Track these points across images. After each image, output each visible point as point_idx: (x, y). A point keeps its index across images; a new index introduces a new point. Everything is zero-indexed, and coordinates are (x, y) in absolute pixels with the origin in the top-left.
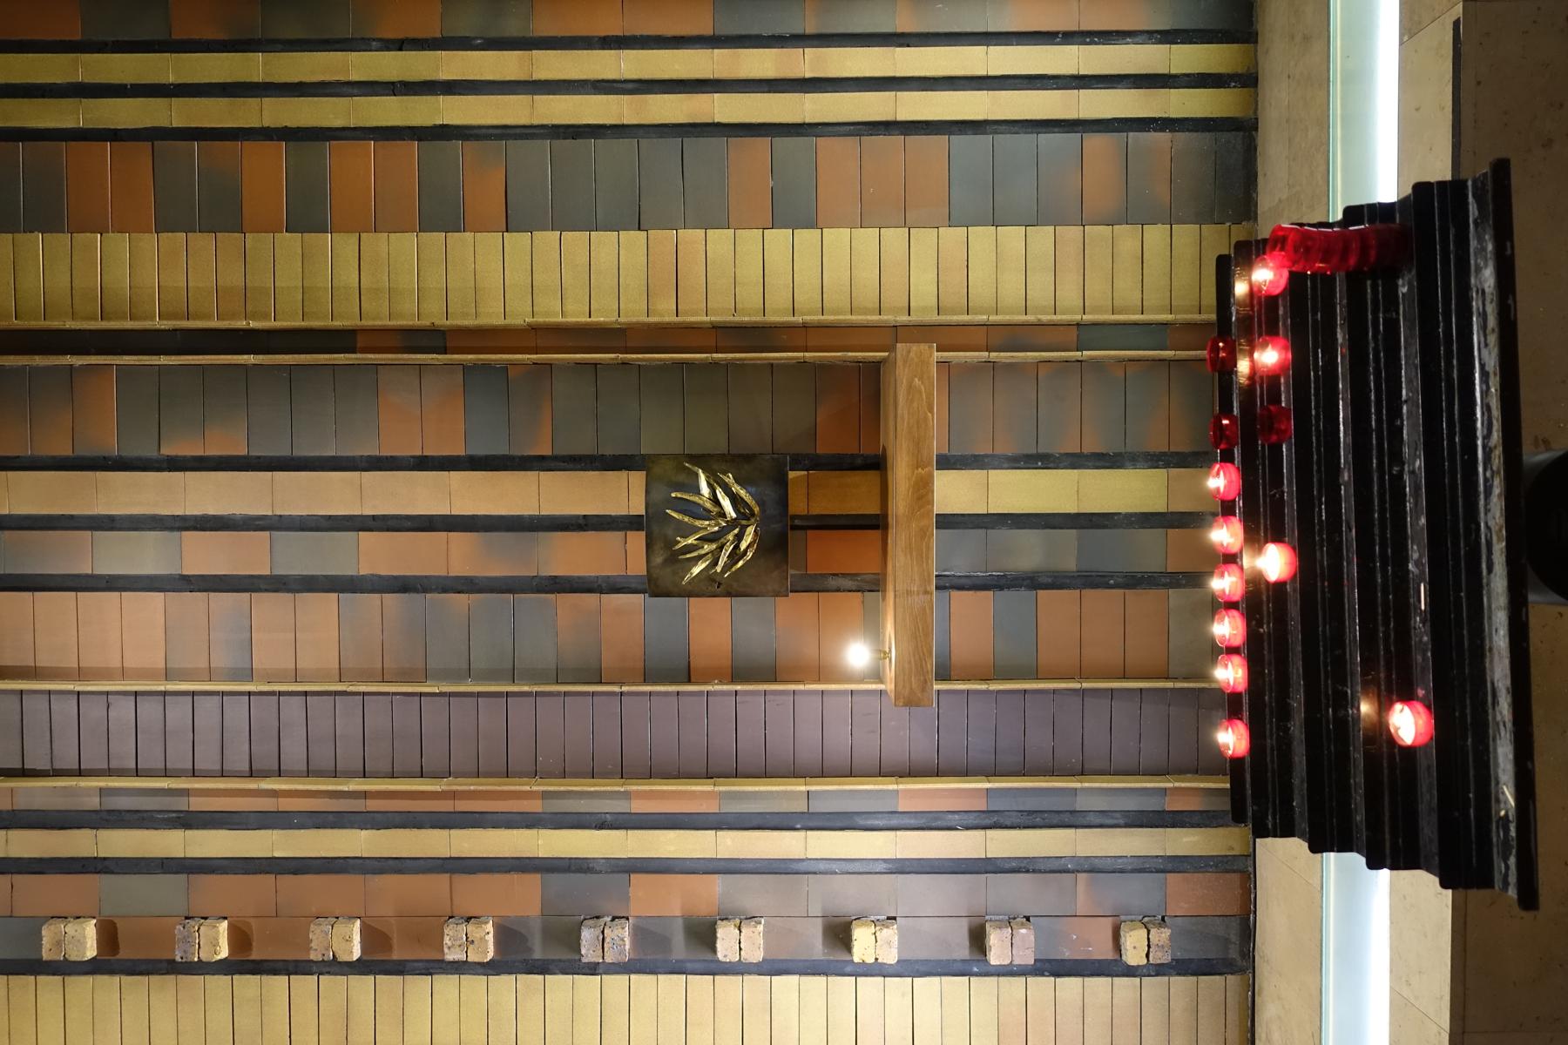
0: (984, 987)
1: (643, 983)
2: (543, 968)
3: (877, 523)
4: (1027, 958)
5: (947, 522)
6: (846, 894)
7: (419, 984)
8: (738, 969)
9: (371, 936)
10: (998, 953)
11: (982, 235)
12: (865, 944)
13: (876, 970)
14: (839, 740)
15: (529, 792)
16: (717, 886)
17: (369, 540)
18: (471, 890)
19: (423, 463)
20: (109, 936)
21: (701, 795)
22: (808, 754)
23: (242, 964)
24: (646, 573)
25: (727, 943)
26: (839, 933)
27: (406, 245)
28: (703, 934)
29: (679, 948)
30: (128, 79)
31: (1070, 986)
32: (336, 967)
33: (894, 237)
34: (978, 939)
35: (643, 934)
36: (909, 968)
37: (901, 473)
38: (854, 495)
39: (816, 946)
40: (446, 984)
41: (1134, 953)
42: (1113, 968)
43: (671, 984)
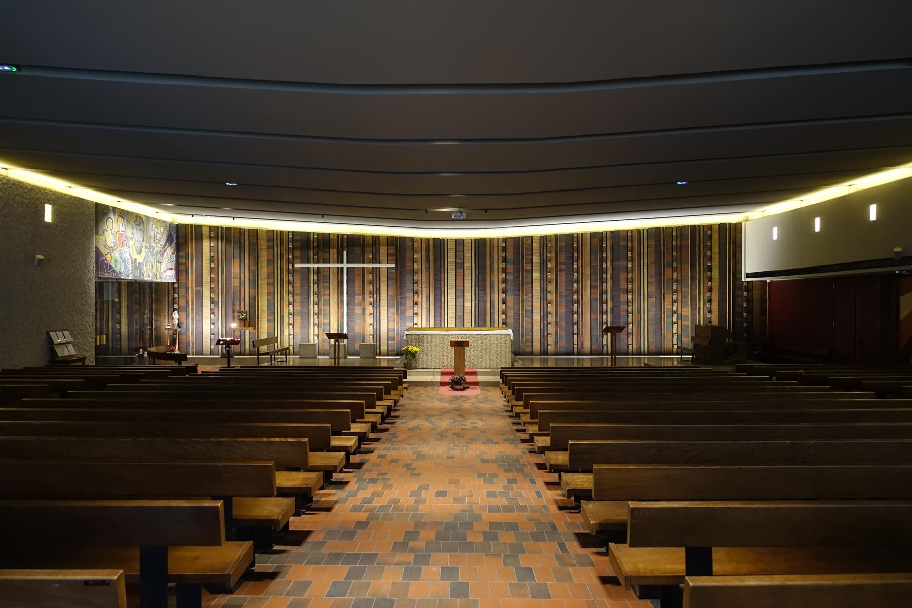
0: (209, 334)
1: (209, 309)
2: (211, 301)
3: (245, 327)
4: (212, 338)
5: (245, 331)
6: (216, 324)
7: (209, 291)
8: (211, 316)
9: (213, 288)
10: (212, 336)
11: (266, 335)
12: (213, 326)
13: (211, 316)
14: (228, 324)
15: (224, 300)
16: (217, 314)
17: (243, 288)
18: (217, 296)
19: (249, 292)
20: (213, 267)
21: (224, 313)
22: (227, 321)
23: (210, 246)
24: (331, 250)
25: (213, 315)
26: (213, 324)
27: (266, 291)
28: (213, 313)
29: (212, 312)
30: (248, 295)
31: (209, 341)
32: (210, 285)
33: (266, 328)
34: (213, 334)
35: (213, 309)
36: (211, 329)
37: (248, 328)
38: (247, 324)
39: (212, 322)
40: (209, 293)
41: (212, 346)
42: (211, 345)
43: (209, 311)
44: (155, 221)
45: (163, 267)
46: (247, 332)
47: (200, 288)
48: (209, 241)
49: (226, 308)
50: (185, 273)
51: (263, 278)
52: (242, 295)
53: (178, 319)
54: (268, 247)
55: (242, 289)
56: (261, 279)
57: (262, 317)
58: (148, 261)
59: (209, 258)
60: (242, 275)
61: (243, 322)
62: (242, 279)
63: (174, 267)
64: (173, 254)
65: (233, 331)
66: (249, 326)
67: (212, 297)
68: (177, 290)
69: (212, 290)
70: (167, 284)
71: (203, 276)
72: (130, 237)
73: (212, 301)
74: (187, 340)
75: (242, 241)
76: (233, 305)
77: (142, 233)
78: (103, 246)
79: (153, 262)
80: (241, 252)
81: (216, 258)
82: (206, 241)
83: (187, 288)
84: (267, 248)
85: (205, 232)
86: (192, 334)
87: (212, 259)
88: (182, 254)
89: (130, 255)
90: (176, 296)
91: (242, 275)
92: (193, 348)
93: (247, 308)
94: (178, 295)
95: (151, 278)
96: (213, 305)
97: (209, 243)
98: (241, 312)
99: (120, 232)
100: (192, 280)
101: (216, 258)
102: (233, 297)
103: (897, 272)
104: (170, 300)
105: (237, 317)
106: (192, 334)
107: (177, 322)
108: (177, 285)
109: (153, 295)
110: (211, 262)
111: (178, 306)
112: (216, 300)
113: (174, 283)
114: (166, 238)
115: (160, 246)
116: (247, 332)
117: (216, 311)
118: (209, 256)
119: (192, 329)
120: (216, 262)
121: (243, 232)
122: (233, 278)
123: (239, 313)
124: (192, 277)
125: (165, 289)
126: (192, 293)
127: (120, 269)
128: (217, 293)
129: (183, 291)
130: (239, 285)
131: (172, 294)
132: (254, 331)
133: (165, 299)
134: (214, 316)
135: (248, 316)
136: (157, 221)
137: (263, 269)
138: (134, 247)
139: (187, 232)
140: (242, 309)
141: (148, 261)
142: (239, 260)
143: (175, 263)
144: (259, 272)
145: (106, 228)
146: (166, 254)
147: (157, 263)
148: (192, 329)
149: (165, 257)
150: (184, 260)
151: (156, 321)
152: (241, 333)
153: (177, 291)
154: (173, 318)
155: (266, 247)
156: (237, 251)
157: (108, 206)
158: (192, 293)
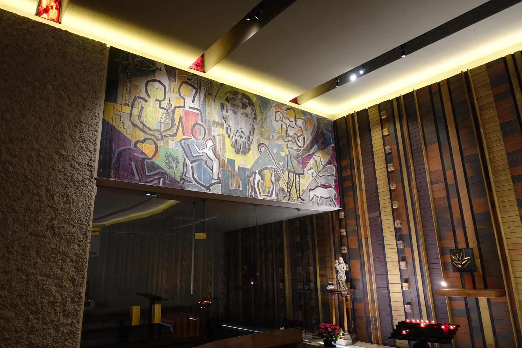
2: (396, 235)
3: (475, 288)
5: (477, 300)
6: (413, 282)
7: (391, 217)
12: (405, 285)
15: (420, 231)
16: (411, 261)
18: (405, 223)
21: (424, 258)
23: (384, 137)
26: (407, 281)
28: (404, 259)
29: (401, 256)
38: (479, 283)
44: (284, 108)
45: (305, 182)
46: (483, 302)
47: (376, 214)
48: (380, 128)
49: (427, 250)
50: (352, 192)
51: (500, 168)
52: (456, 215)
53: (346, 272)
54: (498, 98)
55: (454, 201)
56: (496, 171)
57: (516, 263)
58: (267, 168)
59: (384, 158)
60: (449, 173)
61: (467, 277)
62: (451, 181)
63: (332, 185)
64: (329, 163)
65: (450, 299)
66: (486, 288)
67: (397, 227)
68: (344, 221)
69: (396, 214)
70: (330, 214)
71: (379, 191)
72: (215, 122)
73: (399, 235)
74: (366, 313)
75: (438, 106)
76: (440, 239)
77: (251, 121)
78: (128, 124)
79: (280, 172)
80: (440, 128)
81: (395, 153)
82: (376, 130)
83: (357, 217)
84: (496, 101)
85: (373, 117)
86: (373, 301)
87: (388, 158)
88: (345, 163)
89: (215, 152)
90: (343, 232)
91: (449, 173)
92: (376, 329)
93: (473, 243)
94: (346, 232)
95: (274, 197)
96: (401, 241)
97: (381, 132)
98: (457, 251)
99: (187, 108)
100: (362, 203)
101: (395, 153)
102: (438, 222)
103: (443, 327)
104: (336, 240)
105: (450, 267)
106: (373, 301)
107: (344, 278)
108: (343, 213)
109: (316, 235)
110: (387, 163)
111: (348, 249)
112: (405, 232)
113: (338, 211)
114: (311, 138)
115: (295, 147)
116: (483, 302)
117: (408, 254)
118: (384, 154)
119: (372, 290)
120: (396, 160)
121: (437, 89)
122: (432, 183)
123: (454, 254)
124: (362, 196)
125: (329, 223)
126: (365, 225)
127: (184, 173)
128: (406, 218)
129: (351, 222)
130: (445, 195)
131: (338, 229)
132: (501, 300)
133: (330, 240)
134: (407, 266)
135: (478, 261)
136: (288, 109)
137: (496, 149)
138: (228, 141)
139: (348, 126)
140: (462, 246)
141: (267, 168)
142: (437, 144)
143: (334, 178)
144: (487, 157)
145: (143, 95)
146: (312, 161)
147: (291, 175)
148: (372, 290)
149: (309, 166)
150: (348, 172)
151: (322, 276)
152: (469, 303)
153: (343, 223)
154: (337, 272)
155: (492, 99)
156: (430, 130)
157: (153, 63)
158: (365, 225)
